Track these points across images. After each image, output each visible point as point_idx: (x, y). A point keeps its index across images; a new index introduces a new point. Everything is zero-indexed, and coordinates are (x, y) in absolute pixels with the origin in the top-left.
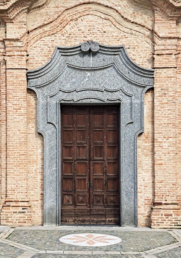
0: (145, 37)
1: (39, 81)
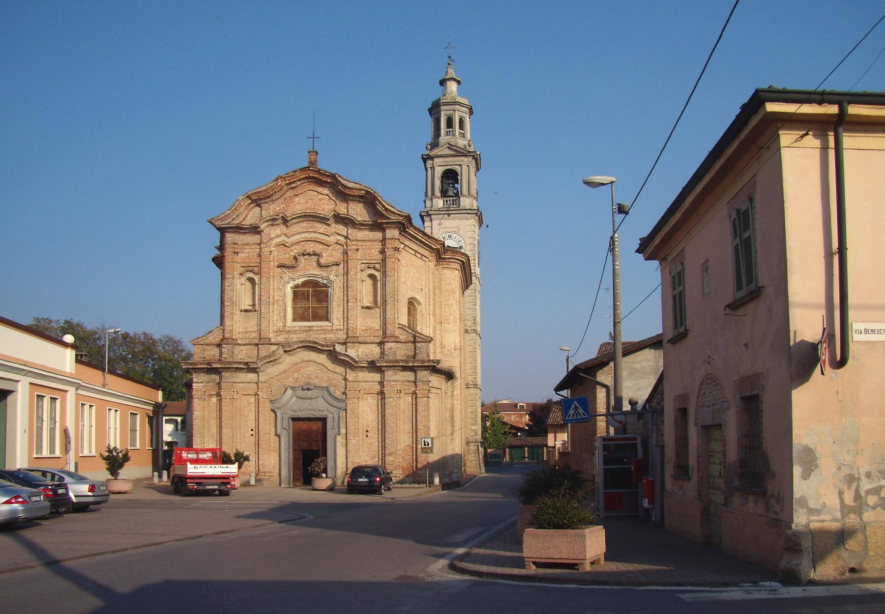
1: (278, 405)
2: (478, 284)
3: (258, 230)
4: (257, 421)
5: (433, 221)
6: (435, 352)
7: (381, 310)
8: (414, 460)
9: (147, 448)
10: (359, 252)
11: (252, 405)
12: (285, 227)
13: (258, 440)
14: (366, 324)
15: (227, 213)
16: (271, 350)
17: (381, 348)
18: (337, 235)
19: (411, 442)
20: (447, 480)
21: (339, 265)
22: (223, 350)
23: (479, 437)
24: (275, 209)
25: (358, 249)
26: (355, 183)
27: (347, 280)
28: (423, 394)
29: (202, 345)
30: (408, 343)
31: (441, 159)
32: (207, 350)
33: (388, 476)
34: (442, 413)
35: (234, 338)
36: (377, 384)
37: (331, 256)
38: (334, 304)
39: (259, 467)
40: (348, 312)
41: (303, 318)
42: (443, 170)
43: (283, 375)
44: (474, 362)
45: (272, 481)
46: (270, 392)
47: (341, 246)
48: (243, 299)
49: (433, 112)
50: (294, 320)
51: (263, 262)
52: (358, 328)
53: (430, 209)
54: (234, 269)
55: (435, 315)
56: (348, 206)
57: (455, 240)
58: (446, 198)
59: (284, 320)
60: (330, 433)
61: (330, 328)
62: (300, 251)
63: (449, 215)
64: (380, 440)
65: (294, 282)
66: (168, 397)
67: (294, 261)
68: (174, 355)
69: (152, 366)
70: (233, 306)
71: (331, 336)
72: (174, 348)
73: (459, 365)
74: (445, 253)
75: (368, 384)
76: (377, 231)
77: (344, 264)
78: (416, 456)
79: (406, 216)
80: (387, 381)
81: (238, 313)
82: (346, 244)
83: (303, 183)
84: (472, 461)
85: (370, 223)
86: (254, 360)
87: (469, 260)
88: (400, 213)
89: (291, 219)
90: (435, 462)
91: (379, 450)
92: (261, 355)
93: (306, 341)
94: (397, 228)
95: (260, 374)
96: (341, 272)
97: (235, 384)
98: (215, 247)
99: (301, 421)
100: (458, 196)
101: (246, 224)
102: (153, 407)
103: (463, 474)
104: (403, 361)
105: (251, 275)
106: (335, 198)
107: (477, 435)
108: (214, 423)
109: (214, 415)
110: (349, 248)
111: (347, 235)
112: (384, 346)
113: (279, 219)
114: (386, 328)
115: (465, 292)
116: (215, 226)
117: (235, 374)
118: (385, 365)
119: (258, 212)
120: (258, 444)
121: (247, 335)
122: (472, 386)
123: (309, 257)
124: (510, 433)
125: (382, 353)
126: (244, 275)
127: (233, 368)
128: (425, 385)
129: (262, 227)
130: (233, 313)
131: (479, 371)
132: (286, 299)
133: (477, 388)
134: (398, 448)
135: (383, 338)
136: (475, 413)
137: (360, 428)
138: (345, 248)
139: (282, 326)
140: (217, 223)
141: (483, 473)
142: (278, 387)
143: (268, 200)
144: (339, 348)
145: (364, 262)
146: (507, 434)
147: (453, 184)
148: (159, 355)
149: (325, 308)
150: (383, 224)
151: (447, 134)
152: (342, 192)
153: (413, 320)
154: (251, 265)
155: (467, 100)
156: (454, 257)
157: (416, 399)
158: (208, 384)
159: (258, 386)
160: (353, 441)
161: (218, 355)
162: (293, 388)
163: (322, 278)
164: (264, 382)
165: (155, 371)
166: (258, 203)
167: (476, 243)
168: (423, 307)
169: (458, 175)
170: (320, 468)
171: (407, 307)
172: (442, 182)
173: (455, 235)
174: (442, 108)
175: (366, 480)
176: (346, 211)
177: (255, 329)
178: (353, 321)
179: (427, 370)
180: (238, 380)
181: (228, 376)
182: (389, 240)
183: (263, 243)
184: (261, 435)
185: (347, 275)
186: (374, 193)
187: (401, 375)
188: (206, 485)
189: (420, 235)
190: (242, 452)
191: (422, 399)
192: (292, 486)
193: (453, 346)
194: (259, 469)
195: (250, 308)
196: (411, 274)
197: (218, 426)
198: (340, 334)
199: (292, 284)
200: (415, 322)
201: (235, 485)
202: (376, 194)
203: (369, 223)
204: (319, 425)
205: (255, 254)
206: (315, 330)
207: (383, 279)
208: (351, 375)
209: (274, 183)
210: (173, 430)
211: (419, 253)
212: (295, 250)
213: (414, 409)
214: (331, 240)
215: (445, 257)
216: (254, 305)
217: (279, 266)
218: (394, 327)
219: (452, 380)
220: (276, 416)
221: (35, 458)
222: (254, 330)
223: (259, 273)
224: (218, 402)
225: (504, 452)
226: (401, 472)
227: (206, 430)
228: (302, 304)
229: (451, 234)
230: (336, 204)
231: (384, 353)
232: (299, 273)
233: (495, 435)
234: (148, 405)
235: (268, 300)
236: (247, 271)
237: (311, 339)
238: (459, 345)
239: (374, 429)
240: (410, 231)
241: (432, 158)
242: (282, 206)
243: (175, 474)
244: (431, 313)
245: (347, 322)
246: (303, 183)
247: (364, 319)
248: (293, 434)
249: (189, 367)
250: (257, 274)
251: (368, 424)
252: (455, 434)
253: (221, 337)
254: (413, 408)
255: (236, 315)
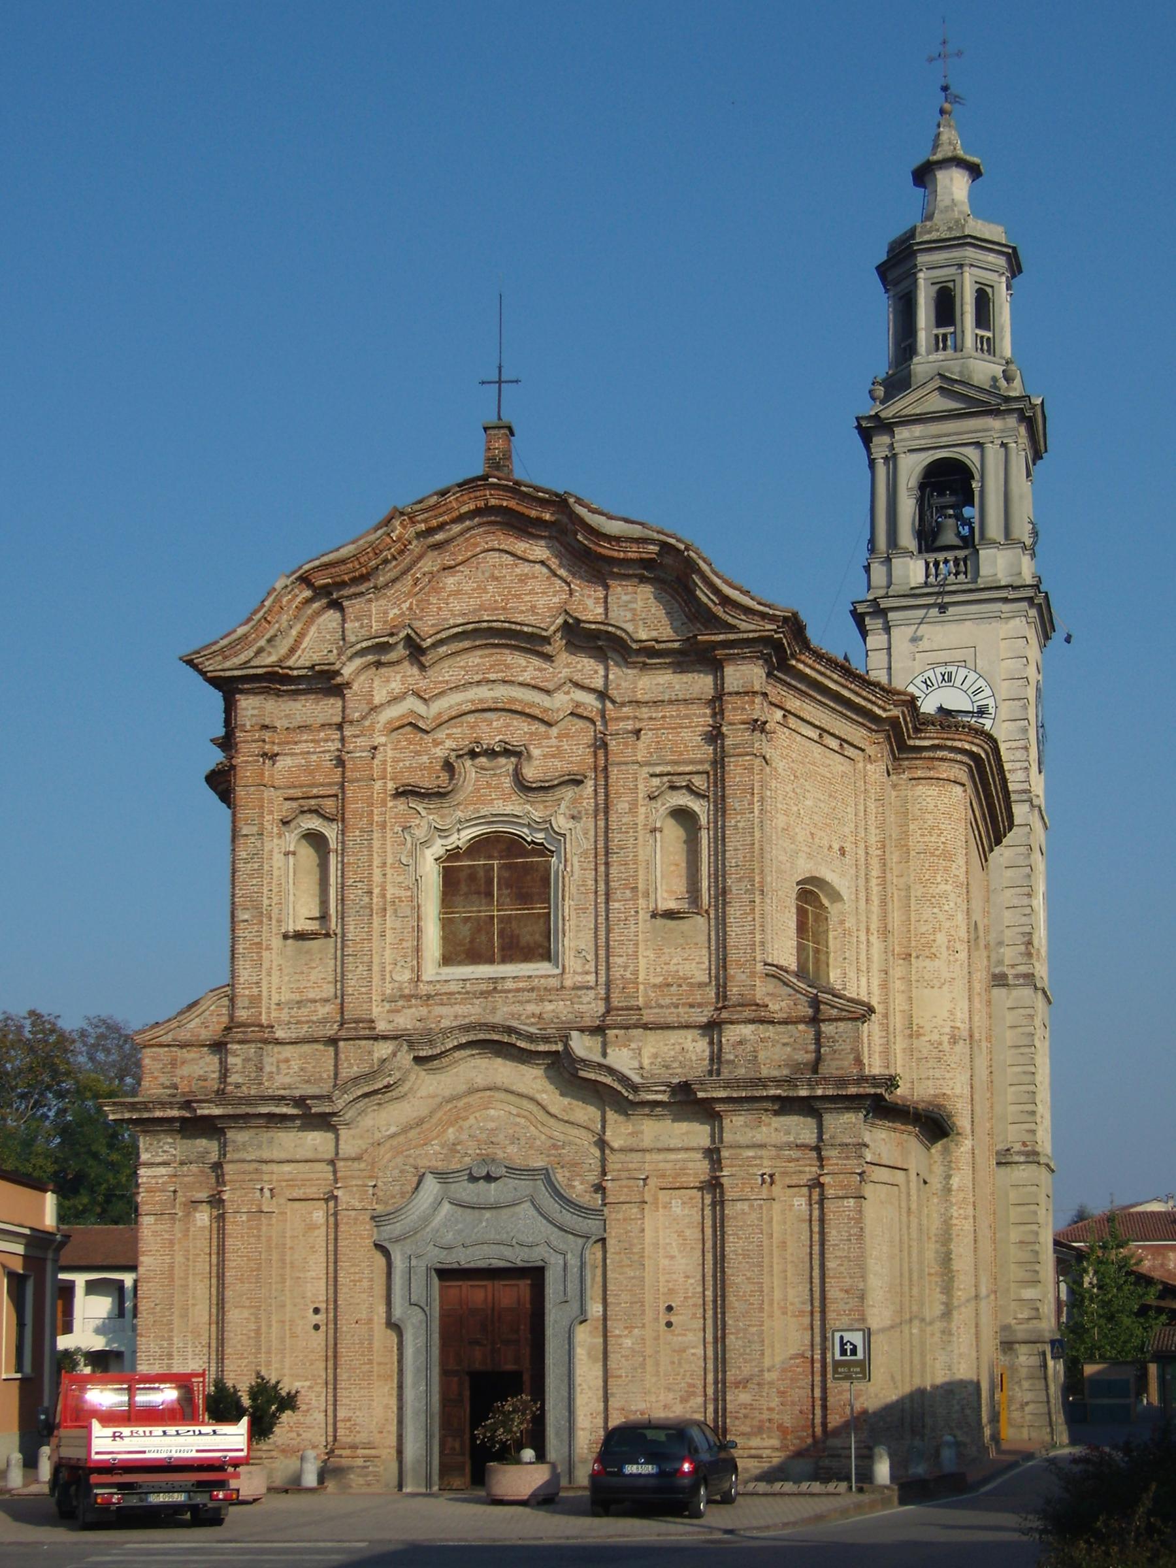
0: (752, 834)
1: (396, 1229)
2: (1038, 825)
3: (333, 682)
4: (331, 1282)
5: (894, 631)
6: (886, 1052)
7: (713, 922)
8: (818, 1403)
9: (4, 1377)
10: (643, 738)
11: (316, 1232)
12: (415, 670)
13: (336, 1344)
14: (665, 967)
15: (241, 631)
16: (376, 1055)
17: (711, 1043)
18: (573, 689)
19: (807, 1342)
20: (919, 1470)
21: (581, 782)
22: (231, 1060)
23: (1048, 1325)
24: (386, 613)
25: (640, 730)
26: (626, 521)
27: (607, 828)
28: (843, 1187)
29: (169, 1046)
30: (795, 1023)
31: (917, 430)
32: (183, 1063)
33: (723, 1455)
34: (910, 1247)
35: (264, 1022)
36: (700, 1156)
37: (558, 754)
38: (568, 907)
39: (335, 1430)
40: (608, 931)
41: (475, 956)
42: (926, 463)
43: (412, 1134)
44: (1027, 1079)
45: (375, 1474)
46: (371, 1191)
47: (588, 724)
48: (291, 898)
49: (892, 275)
50: (447, 960)
51: (352, 781)
52: (641, 980)
53: (882, 592)
54: (262, 807)
55: (885, 932)
56: (606, 597)
57: (965, 687)
58: (935, 555)
59: (415, 962)
60: (555, 1319)
61: (554, 983)
62: (462, 743)
63: (943, 608)
64: (709, 1338)
65: (444, 842)
66: (104, 1211)
67: (444, 776)
68: (122, 1079)
69: (57, 1114)
70: (261, 922)
71: (557, 1009)
72: (124, 1057)
73: (967, 1091)
74: (917, 730)
75: (672, 1156)
76: (700, 672)
77: (595, 779)
78: (824, 1389)
79: (786, 619)
80: (731, 1147)
81: (276, 942)
82: (603, 717)
83: (469, 529)
84: (1023, 1405)
85: (676, 645)
86: (324, 1088)
87: (996, 750)
88: (766, 610)
89: (434, 645)
90: (889, 1409)
91: (705, 1369)
92: (345, 1073)
93: (481, 1025)
94: (758, 658)
95: (343, 1133)
96: (588, 804)
97: (264, 1167)
98: (211, 741)
99: (470, 1279)
100: (974, 546)
101: (299, 664)
102: (27, 1246)
103: (986, 1449)
104: (778, 1082)
105: (313, 823)
106: (569, 571)
107: (1038, 1318)
108: (201, 1292)
109: (203, 1265)
110: (613, 727)
111: (606, 684)
112: (720, 1036)
113: (397, 643)
114: (725, 978)
115: (991, 856)
116: (203, 673)
117: (265, 1136)
118: (722, 1094)
119: (334, 624)
120: (335, 1357)
121: (304, 1011)
122: (1022, 1159)
123: (489, 760)
124: (1160, 1310)
125: (716, 1058)
126: (293, 825)
127: (260, 1115)
128: (847, 1158)
129: (347, 671)
130: (260, 943)
131: (1044, 1109)
132: (422, 896)
133: (1039, 1163)
134: (767, 1362)
135: (717, 1009)
136: (1030, 1248)
137: (648, 1298)
138: (600, 728)
139: (411, 980)
140: (212, 666)
141: (1062, 1446)
142: (396, 1172)
143: (362, 588)
144: (583, 1046)
145: (658, 770)
146: (1152, 1313)
147: (957, 507)
148: (77, 1082)
149: (542, 920)
150: (714, 649)
151: (940, 343)
152: (587, 550)
153: (817, 951)
154: (315, 791)
155: (1000, 229)
156: (949, 743)
157: (821, 1202)
158: (185, 1168)
159: (335, 1172)
160: (625, 1342)
161: (216, 1075)
162: (442, 1176)
163: (529, 826)
164: (354, 1159)
165: (65, 1131)
166: (335, 596)
167: (1031, 693)
168: (848, 905)
169: (973, 478)
170: (511, 1431)
171: (794, 910)
172: (921, 502)
173: (962, 672)
174: (922, 259)
175: (649, 1469)
176: (601, 610)
177: (328, 990)
178: (624, 959)
179: (857, 1110)
180: (277, 1154)
181: (244, 1144)
182: (738, 701)
183: (351, 722)
184: (344, 1326)
185: (606, 813)
186: (687, 549)
187: (774, 1125)
188: (147, 1493)
189: (835, 677)
190: (273, 1382)
191: (840, 1202)
192: (435, 1488)
193: (947, 1030)
194: (335, 1437)
195: (313, 926)
196: (807, 803)
197: (214, 1301)
198: (585, 999)
199: (438, 848)
200: (823, 957)
201: (238, 1490)
202: (692, 554)
203: (670, 645)
204: (524, 1286)
205: (327, 756)
206: (509, 991)
207: (716, 822)
208: (619, 1130)
209: (380, 532)
210: (109, 1313)
211: (833, 735)
212: (448, 741)
213: (816, 1237)
214: (558, 705)
215: (918, 743)
216: (324, 917)
217: (398, 794)
218: (753, 974)
219: (945, 1140)
220: (389, 1265)
221: (5, 1380)
222: (324, 995)
223: (338, 818)
224: (215, 1225)
225: (1143, 1377)
226: (775, 1442)
227: (177, 1313)
228: (476, 909)
229: (950, 669)
230: (571, 590)
231: (719, 1058)
232: (460, 814)
233: (1111, 1318)
234: (11, 1238)
235: (366, 899)
236: (303, 812)
237: (497, 1019)
238: (968, 1027)
239: (691, 1302)
240: (801, 666)
241: (886, 427)
242: (407, 604)
243: (61, 1458)
244: (874, 927)
245: (607, 962)
246: (469, 529)
247: (659, 951)
248: (441, 1320)
249: (127, 1116)
250: (333, 820)
251: (671, 1285)
252: (955, 1313)
253: (225, 1019)
254: (811, 1231)
255: (268, 948)
